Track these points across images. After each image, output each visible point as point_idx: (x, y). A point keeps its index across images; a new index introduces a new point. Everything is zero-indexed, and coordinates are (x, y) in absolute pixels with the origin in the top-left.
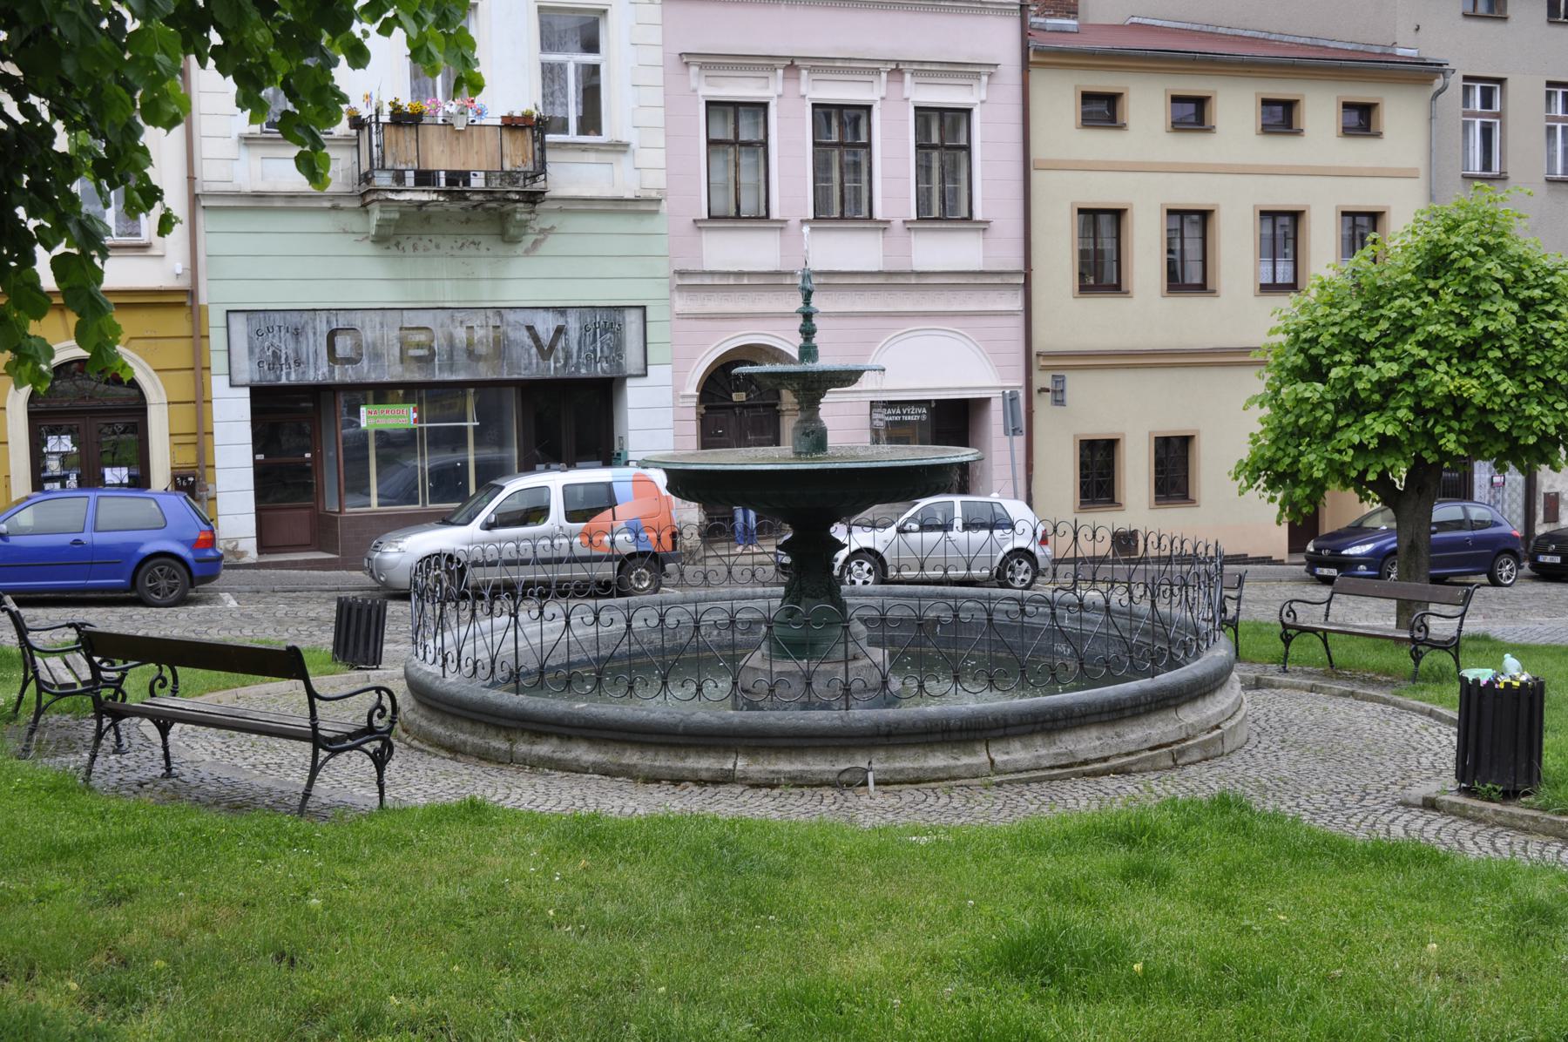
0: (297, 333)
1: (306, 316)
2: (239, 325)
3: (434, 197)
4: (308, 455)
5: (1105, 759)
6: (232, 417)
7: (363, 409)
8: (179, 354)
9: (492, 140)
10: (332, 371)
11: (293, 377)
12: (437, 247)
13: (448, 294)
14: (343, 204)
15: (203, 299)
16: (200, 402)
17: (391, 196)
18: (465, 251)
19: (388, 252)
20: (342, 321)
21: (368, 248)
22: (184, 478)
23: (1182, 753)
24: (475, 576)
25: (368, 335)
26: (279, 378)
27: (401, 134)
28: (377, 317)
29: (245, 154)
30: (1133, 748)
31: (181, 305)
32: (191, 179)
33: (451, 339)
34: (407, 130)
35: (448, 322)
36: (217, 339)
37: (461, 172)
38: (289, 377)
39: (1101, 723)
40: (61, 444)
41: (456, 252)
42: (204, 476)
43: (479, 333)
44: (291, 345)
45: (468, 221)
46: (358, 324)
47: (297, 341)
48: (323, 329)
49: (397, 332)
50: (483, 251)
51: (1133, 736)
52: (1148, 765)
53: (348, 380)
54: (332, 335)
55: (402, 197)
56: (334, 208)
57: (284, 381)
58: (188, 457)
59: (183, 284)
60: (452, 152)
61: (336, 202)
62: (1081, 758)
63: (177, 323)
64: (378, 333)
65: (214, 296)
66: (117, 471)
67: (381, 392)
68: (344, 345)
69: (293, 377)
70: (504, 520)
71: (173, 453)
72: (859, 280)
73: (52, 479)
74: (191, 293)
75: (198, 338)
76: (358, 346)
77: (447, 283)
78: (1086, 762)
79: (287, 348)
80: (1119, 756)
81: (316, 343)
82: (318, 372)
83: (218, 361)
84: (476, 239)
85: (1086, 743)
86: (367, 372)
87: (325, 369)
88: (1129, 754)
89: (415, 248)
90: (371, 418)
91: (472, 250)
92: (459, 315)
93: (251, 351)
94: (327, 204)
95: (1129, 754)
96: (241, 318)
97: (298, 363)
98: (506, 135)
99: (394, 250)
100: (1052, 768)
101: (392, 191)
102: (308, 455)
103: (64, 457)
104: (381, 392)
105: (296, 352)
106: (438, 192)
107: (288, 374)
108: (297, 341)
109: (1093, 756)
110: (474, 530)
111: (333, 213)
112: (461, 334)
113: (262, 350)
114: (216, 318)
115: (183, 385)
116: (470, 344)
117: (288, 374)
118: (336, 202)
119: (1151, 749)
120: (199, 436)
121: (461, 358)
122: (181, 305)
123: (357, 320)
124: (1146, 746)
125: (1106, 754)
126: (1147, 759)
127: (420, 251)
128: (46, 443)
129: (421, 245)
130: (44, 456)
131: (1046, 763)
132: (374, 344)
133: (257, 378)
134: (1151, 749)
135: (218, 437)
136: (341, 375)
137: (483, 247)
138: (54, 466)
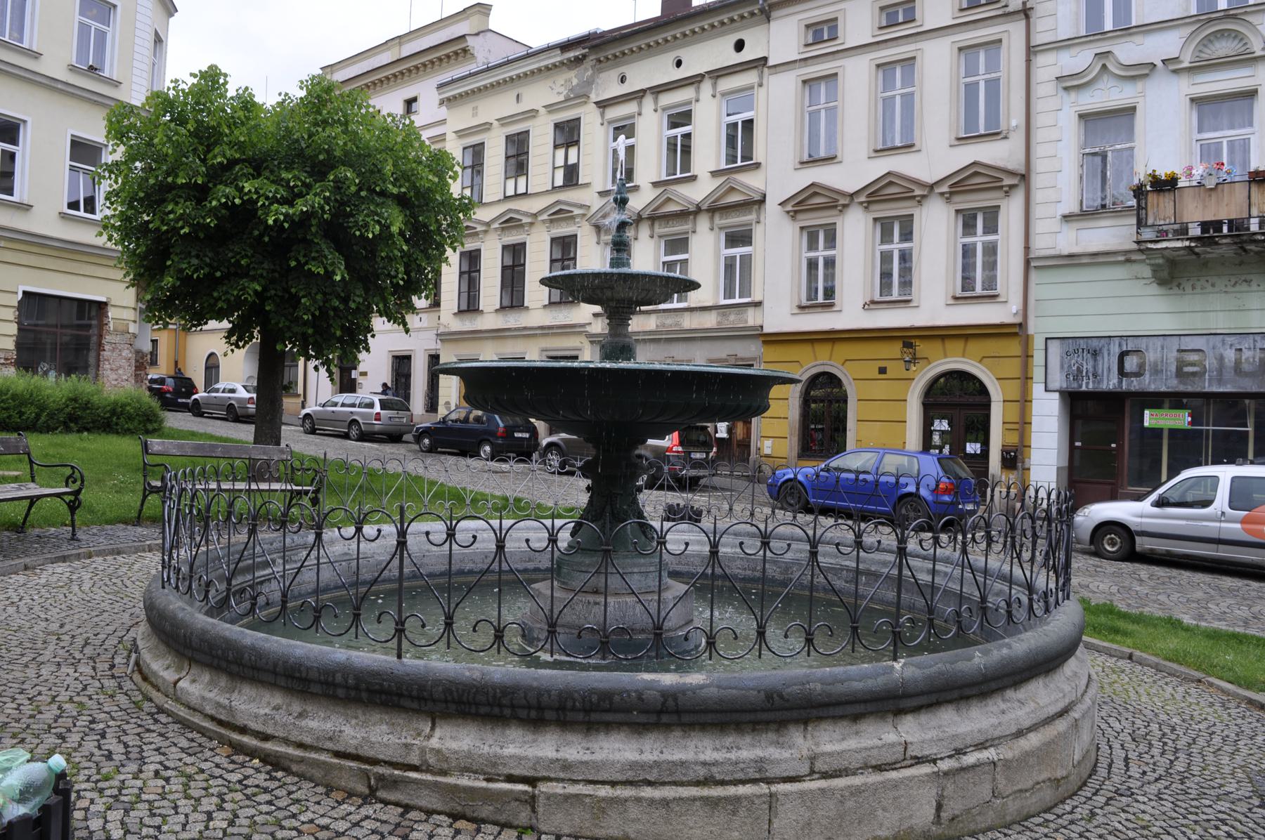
0: (1095, 354)
1: (1103, 341)
2: (1055, 348)
3: (1187, 243)
4: (1113, 445)
5: (266, 737)
6: (1047, 416)
7: (1147, 412)
8: (1013, 368)
9: (1240, 192)
10: (1120, 382)
11: (1091, 386)
12: (1213, 285)
13: (1220, 322)
14: (1134, 257)
15: (1031, 331)
16: (1024, 401)
17: (1150, 246)
18: (1238, 288)
19: (1171, 292)
20: (1131, 346)
21: (1154, 289)
22: (1008, 453)
23: (395, 783)
24: (1142, 544)
25: (1151, 357)
26: (1081, 386)
27: (1161, 198)
28: (1159, 342)
29: (1065, 227)
30: (308, 740)
31: (1016, 334)
32: (1027, 248)
33: (1221, 359)
34: (1167, 194)
35: (1220, 345)
36: (1038, 358)
37: (1211, 222)
38: (1087, 386)
39: (288, 690)
40: (942, 425)
41: (1230, 289)
42: (1022, 454)
43: (1247, 354)
44: (1091, 363)
45: (1241, 263)
46: (1143, 347)
47: (1095, 360)
48: (1116, 350)
49: (1175, 354)
50: (1254, 287)
51: (313, 724)
52: (318, 774)
53: (1133, 389)
54: (1122, 356)
55: (1159, 246)
56: (1128, 261)
57: (1084, 388)
58: (1013, 439)
59: (1018, 320)
60: (1205, 207)
61: (1128, 256)
62: (241, 721)
63: (1014, 347)
64: (1159, 355)
65: (1038, 328)
66: (973, 445)
67: (1156, 400)
68: (1131, 363)
69: (1091, 386)
70: (1161, 503)
71: (1003, 435)
72: (95, 98)
73: (935, 447)
74: (1022, 326)
75: (1027, 356)
76: (1142, 366)
77: (1221, 314)
78: (243, 730)
79: (1088, 366)
80: (286, 741)
81: (1109, 362)
82: (1110, 382)
83: (1038, 373)
84: (1248, 277)
85: (254, 705)
86: (1148, 383)
87: (1116, 381)
88: (300, 745)
89: (1193, 288)
90: (1150, 419)
91: (1244, 287)
92: (1229, 340)
93: (1062, 367)
94: (1121, 258)
95: (300, 745)
96: (1057, 343)
97: (1095, 376)
98: (1254, 188)
99: (1176, 290)
100: (213, 718)
101: (1151, 242)
102: (1113, 445)
103: (943, 432)
104: (1156, 400)
105: (1094, 367)
106: (1191, 239)
107: (1087, 384)
108: (1095, 360)
109: (253, 725)
110: (1146, 506)
111: (1128, 265)
112: (1230, 355)
113: (1070, 366)
114: (1038, 344)
115: (1014, 390)
116: (1238, 363)
117: (1087, 384)
118: (1128, 256)
119: (338, 754)
120: (1022, 425)
121: (1229, 374)
122: (1016, 334)
123: (1142, 344)
124: (329, 745)
125: (270, 731)
126: (327, 767)
127: (1198, 290)
128: (932, 424)
129: (1198, 284)
130: (931, 432)
131: (209, 710)
132: (1156, 364)
133: (1065, 385)
134: (338, 754)
135: (1034, 427)
136: (1135, 385)
137: (1254, 284)
138: (936, 439)
